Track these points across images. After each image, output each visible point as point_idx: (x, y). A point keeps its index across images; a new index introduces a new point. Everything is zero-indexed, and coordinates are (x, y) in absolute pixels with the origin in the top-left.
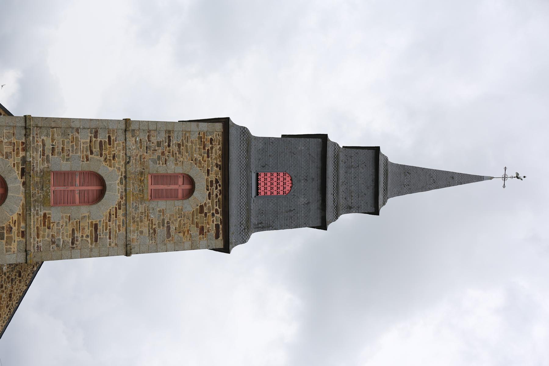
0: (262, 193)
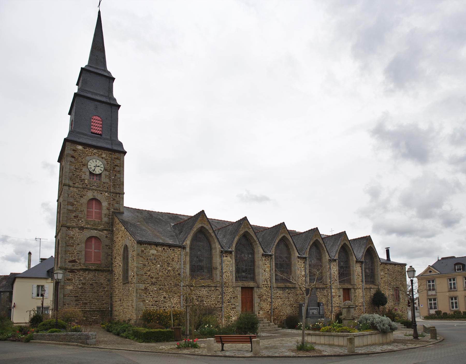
0: (101, 132)
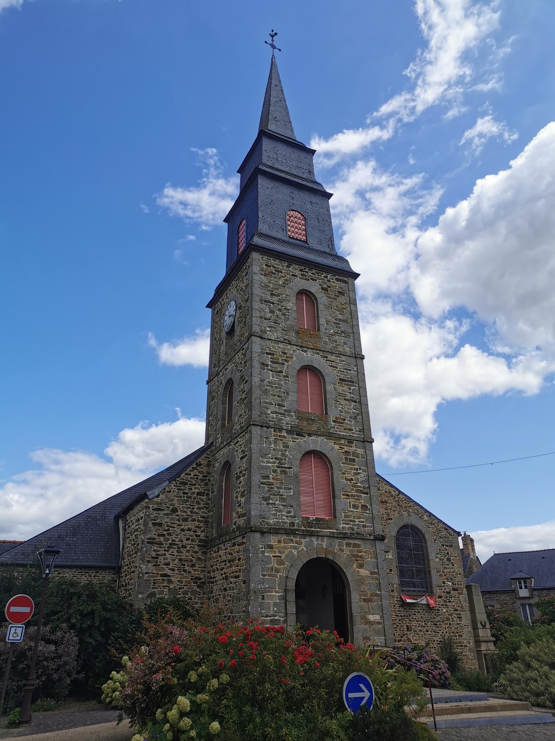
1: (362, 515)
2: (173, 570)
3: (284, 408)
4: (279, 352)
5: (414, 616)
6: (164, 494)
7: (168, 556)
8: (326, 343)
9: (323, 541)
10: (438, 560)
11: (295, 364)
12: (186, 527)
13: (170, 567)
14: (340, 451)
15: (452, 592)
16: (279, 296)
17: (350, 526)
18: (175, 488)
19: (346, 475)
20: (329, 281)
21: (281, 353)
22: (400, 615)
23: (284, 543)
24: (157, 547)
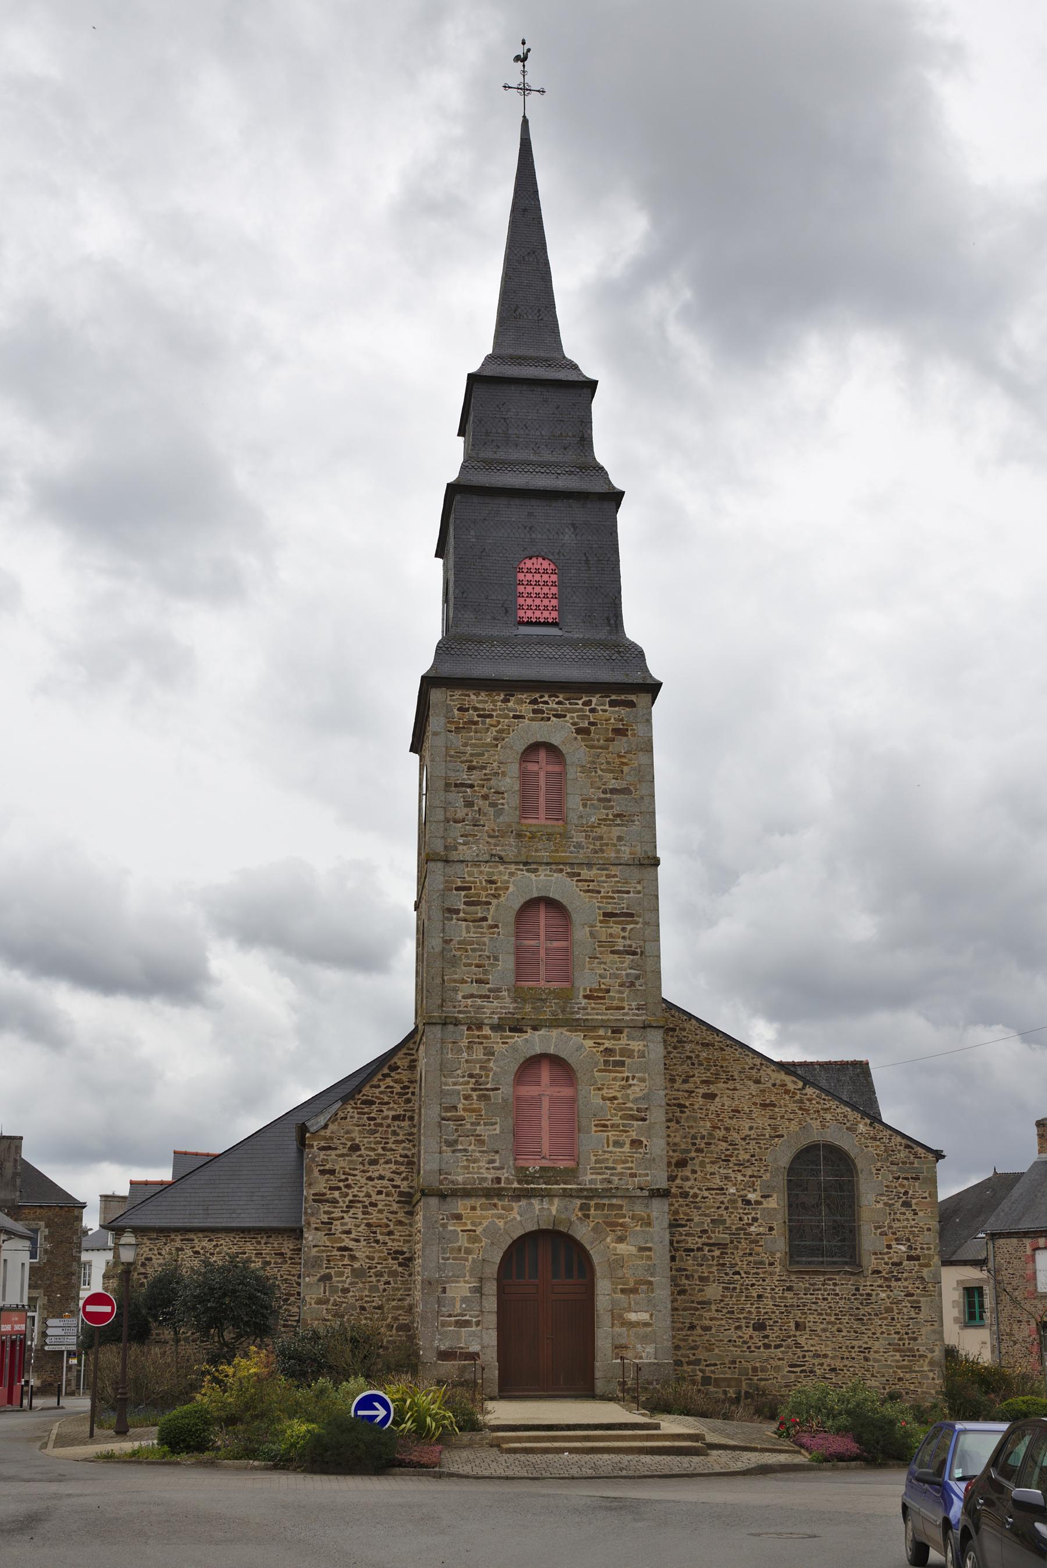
0: (555, 614)
1: (630, 1157)
2: (357, 1241)
3: (488, 986)
4: (481, 883)
5: (814, 1305)
6: (336, 1123)
7: (347, 1220)
8: (579, 846)
9: (551, 1203)
10: (880, 1205)
11: (513, 898)
12: (376, 1174)
13: (353, 1236)
14: (595, 1050)
15: (905, 1263)
16: (485, 768)
17: (604, 1176)
18: (353, 1112)
19: (604, 1092)
20: (593, 711)
21: (484, 883)
22: (783, 1304)
23: (482, 1209)
24: (329, 1207)
